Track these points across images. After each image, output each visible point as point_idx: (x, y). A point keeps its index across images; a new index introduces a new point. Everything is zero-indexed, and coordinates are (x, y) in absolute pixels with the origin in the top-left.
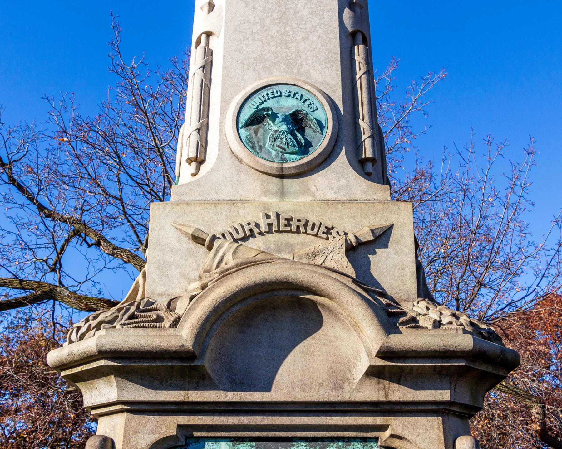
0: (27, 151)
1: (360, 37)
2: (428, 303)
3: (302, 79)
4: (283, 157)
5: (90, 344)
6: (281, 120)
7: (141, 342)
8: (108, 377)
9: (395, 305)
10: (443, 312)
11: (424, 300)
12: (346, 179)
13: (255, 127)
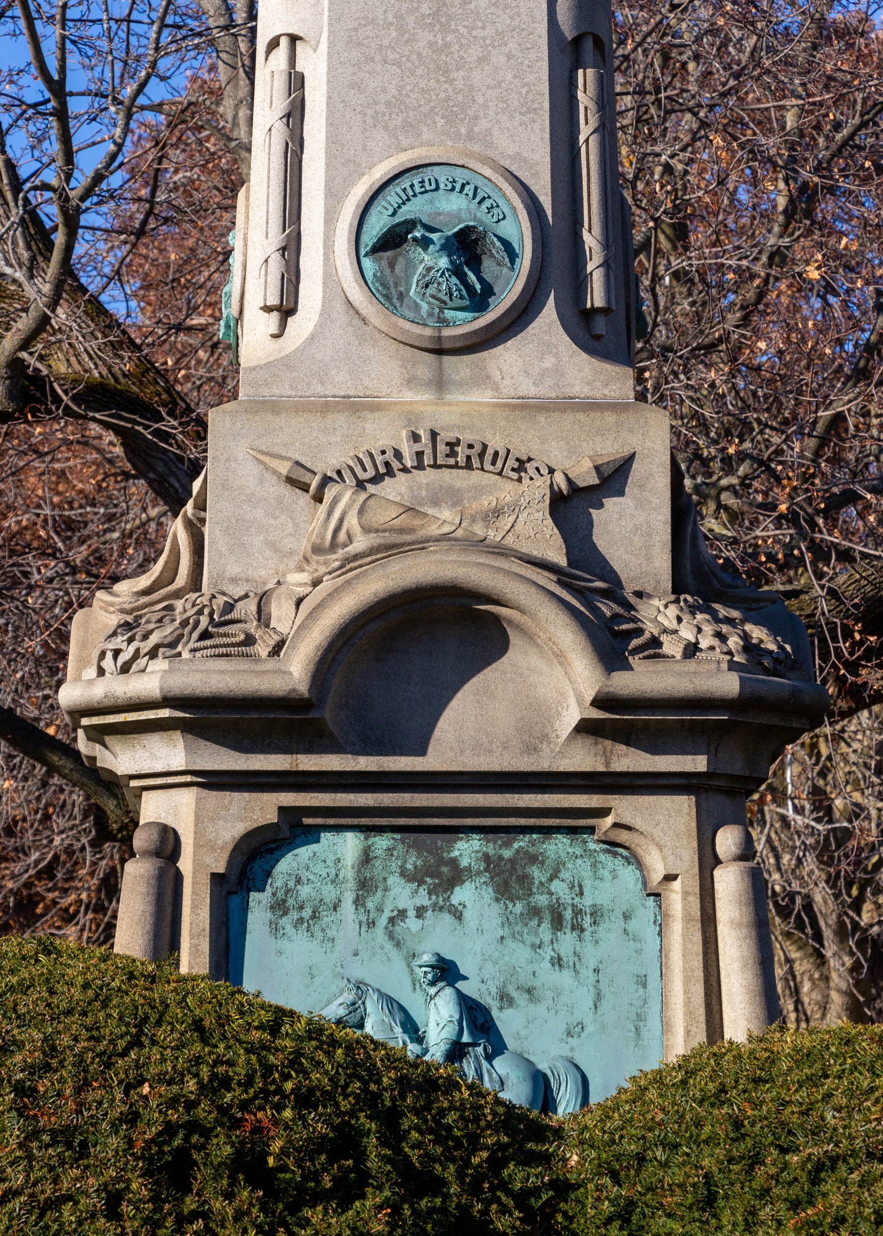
1: (589, 44)
6: (438, 247)
12: (556, 355)
13: (389, 254)
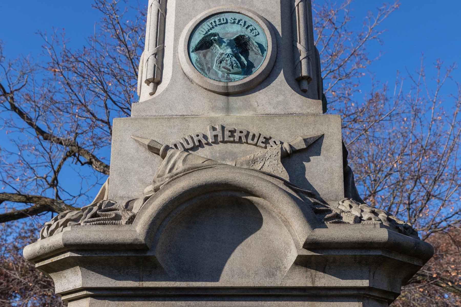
0: (27, 82)
2: (351, 202)
3: (246, 7)
4: (228, 77)
5: (57, 239)
6: (226, 44)
7: (101, 237)
8: (74, 268)
9: (322, 203)
10: (364, 210)
11: (349, 199)
13: (204, 51)
